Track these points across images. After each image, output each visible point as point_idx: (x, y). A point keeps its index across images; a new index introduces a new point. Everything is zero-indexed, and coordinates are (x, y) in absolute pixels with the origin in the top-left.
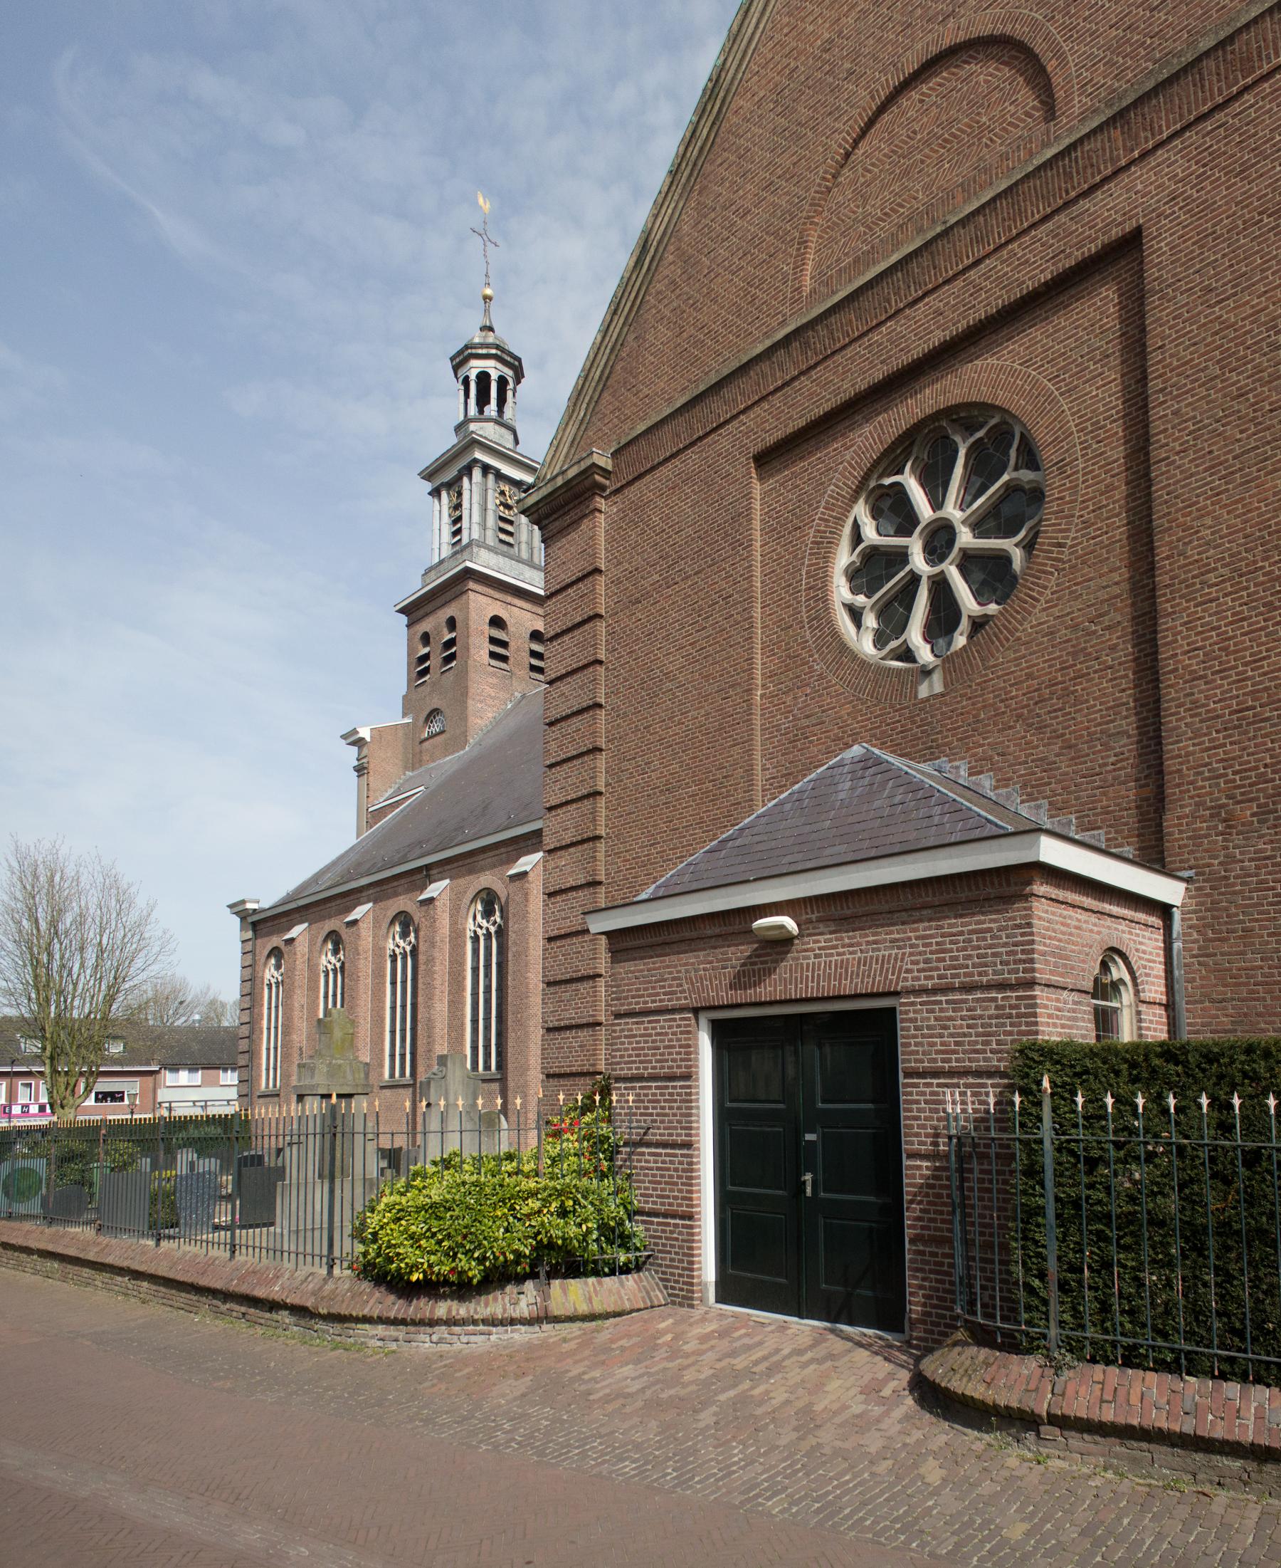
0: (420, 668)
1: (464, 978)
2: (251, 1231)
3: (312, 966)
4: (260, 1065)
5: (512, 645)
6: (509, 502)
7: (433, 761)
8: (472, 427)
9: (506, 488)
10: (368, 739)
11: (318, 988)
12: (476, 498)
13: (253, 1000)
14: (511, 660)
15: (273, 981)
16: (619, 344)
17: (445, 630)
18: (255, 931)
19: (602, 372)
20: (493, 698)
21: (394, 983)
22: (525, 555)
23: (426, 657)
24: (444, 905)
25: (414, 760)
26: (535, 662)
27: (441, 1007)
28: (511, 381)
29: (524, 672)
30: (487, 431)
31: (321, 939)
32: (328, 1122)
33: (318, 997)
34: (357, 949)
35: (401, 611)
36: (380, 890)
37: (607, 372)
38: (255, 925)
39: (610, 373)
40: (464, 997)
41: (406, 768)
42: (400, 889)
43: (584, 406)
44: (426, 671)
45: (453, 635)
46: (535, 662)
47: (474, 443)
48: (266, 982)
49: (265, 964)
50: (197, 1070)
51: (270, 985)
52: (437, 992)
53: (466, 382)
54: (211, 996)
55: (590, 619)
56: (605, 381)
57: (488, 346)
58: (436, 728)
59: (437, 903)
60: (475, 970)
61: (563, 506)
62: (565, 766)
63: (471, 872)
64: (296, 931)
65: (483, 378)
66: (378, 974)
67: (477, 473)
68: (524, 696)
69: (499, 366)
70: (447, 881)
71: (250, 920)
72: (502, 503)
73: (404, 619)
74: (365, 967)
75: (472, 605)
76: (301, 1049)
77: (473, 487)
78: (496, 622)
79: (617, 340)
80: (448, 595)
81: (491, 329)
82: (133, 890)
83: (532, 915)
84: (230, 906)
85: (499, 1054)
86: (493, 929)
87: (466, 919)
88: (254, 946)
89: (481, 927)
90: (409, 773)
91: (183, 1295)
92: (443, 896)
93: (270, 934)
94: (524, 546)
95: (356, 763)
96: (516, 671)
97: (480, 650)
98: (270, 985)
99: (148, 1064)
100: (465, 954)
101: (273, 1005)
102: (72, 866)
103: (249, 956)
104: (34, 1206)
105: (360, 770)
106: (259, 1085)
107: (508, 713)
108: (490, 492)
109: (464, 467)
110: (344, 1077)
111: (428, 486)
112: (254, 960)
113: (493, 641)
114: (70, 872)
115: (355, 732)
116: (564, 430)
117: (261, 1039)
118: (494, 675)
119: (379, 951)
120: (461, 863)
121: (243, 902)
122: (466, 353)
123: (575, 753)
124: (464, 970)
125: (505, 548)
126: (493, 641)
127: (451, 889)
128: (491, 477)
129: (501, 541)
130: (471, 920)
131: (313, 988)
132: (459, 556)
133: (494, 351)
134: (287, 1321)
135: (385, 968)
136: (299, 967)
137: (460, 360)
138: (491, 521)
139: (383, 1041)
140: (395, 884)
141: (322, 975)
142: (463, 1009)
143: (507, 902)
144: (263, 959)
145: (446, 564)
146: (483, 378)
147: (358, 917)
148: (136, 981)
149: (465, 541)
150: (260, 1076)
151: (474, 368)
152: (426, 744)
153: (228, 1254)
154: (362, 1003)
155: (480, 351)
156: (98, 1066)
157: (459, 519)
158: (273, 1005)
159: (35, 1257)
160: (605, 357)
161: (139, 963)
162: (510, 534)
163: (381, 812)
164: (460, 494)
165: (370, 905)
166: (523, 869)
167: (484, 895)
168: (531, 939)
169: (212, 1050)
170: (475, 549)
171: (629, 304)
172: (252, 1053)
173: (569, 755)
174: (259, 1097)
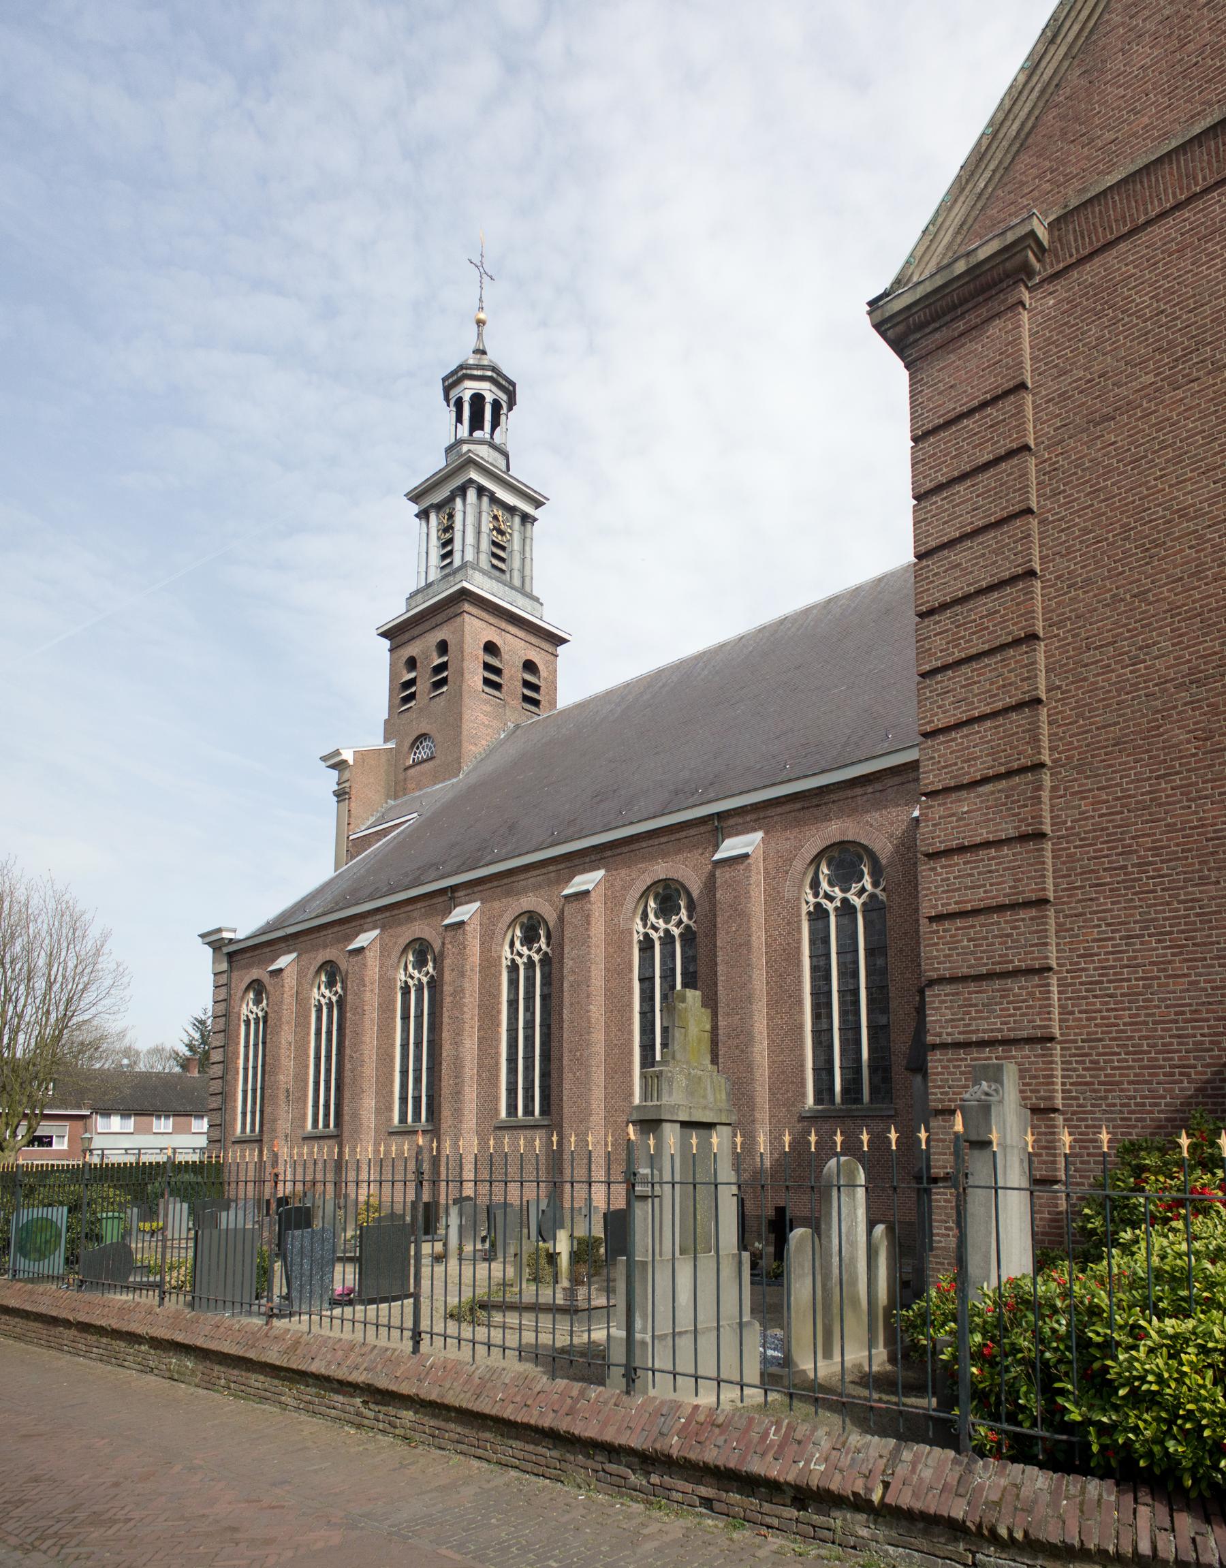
0: (404, 693)
1: (499, 1012)
2: (384, 1306)
3: (301, 1000)
4: (235, 1108)
5: (506, 673)
6: (502, 527)
7: (420, 789)
8: (465, 448)
9: (500, 513)
10: (351, 762)
11: (309, 1024)
12: (470, 519)
13: (227, 1038)
14: (505, 689)
15: (252, 1017)
16: (1057, 82)
17: (435, 654)
18: (230, 962)
19: (1023, 124)
20: (487, 726)
21: (405, 1018)
22: (517, 582)
23: (412, 682)
24: (475, 930)
25: (397, 788)
26: (528, 693)
27: (471, 1044)
28: (504, 405)
29: (517, 702)
30: (483, 453)
31: (313, 969)
32: (412, 1166)
33: (308, 1034)
34: (363, 980)
35: (384, 635)
36: (387, 916)
37: (1030, 124)
38: (230, 956)
39: (1033, 127)
40: (498, 1033)
41: (388, 797)
42: (415, 914)
43: (988, 174)
44: (412, 697)
45: (445, 659)
46: (528, 693)
47: (470, 462)
48: (243, 1018)
49: (242, 999)
50: (129, 1116)
51: (247, 1022)
52: (467, 1026)
53: (459, 403)
54: (126, 1042)
55: (1011, 454)
56: (1022, 142)
57: (483, 368)
58: (423, 754)
59: (468, 928)
60: (513, 1003)
61: (955, 307)
62: (965, 669)
63: (508, 894)
64: (283, 962)
65: (478, 399)
66: (386, 1007)
67: (471, 494)
68: (517, 727)
69: (494, 389)
70: (477, 905)
71: (226, 950)
72: (495, 528)
73: (387, 643)
74: (371, 999)
75: (467, 628)
76: (287, 1091)
77: (467, 511)
78: (490, 648)
79: (1051, 78)
80: (439, 618)
81: (484, 352)
82: (87, 917)
83: (594, 940)
84: (202, 936)
85: (545, 1097)
86: (334, 999)
87: (502, 945)
88: (229, 978)
89: (412, 978)
90: (391, 802)
91: (515, 1444)
92: (473, 920)
93: (249, 966)
94: (516, 574)
95: (336, 788)
96: (509, 700)
97: (474, 677)
98: (247, 1022)
99: (79, 1108)
100: (500, 984)
101: (252, 1043)
102: (23, 890)
103: (224, 990)
104: (56, 1263)
105: (341, 795)
106: (234, 1130)
107: (502, 743)
108: (484, 515)
109: (458, 488)
110: (705, 1097)
111: (415, 509)
112: (229, 993)
113: (487, 667)
114: (20, 894)
115: (337, 753)
116: (950, 209)
117: (236, 1080)
118: (487, 702)
119: (387, 983)
120: (495, 884)
121: (219, 930)
122: (460, 374)
123: (986, 647)
124: (499, 1003)
125: (497, 573)
126: (487, 667)
127: (482, 913)
128: (485, 500)
129: (494, 566)
130: (507, 947)
131: (302, 1023)
132: (451, 578)
133: (489, 373)
134: (864, 1532)
135: (395, 1002)
136: (286, 1001)
137: (452, 382)
138: (485, 545)
139: (392, 1082)
140: (409, 908)
141: (314, 1010)
142: (498, 1047)
143: (442, 953)
144: (240, 993)
145: (435, 587)
146: (478, 399)
147: (365, 944)
148: (86, 1017)
149: (457, 562)
150: (235, 1120)
151: (469, 389)
152: (412, 771)
153: (408, 1345)
154: (367, 1039)
155: (475, 372)
156: (43, 1107)
157: (450, 541)
158: (252, 1043)
159: (144, 1348)
160: (1029, 105)
161: (89, 996)
162: (502, 560)
163: (365, 842)
164: (451, 516)
165: (376, 932)
166: (584, 888)
167: (525, 919)
168: (593, 967)
169: (146, 1097)
170: (470, 572)
171: (1076, 28)
172: (226, 1095)
173: (974, 651)
174: (234, 1142)
